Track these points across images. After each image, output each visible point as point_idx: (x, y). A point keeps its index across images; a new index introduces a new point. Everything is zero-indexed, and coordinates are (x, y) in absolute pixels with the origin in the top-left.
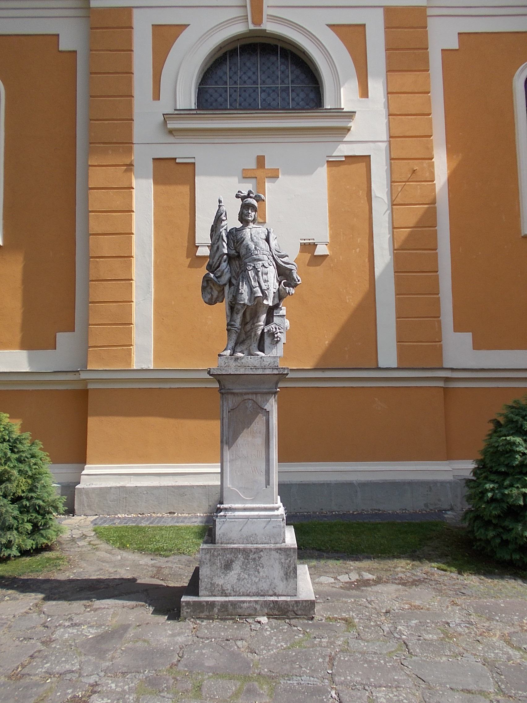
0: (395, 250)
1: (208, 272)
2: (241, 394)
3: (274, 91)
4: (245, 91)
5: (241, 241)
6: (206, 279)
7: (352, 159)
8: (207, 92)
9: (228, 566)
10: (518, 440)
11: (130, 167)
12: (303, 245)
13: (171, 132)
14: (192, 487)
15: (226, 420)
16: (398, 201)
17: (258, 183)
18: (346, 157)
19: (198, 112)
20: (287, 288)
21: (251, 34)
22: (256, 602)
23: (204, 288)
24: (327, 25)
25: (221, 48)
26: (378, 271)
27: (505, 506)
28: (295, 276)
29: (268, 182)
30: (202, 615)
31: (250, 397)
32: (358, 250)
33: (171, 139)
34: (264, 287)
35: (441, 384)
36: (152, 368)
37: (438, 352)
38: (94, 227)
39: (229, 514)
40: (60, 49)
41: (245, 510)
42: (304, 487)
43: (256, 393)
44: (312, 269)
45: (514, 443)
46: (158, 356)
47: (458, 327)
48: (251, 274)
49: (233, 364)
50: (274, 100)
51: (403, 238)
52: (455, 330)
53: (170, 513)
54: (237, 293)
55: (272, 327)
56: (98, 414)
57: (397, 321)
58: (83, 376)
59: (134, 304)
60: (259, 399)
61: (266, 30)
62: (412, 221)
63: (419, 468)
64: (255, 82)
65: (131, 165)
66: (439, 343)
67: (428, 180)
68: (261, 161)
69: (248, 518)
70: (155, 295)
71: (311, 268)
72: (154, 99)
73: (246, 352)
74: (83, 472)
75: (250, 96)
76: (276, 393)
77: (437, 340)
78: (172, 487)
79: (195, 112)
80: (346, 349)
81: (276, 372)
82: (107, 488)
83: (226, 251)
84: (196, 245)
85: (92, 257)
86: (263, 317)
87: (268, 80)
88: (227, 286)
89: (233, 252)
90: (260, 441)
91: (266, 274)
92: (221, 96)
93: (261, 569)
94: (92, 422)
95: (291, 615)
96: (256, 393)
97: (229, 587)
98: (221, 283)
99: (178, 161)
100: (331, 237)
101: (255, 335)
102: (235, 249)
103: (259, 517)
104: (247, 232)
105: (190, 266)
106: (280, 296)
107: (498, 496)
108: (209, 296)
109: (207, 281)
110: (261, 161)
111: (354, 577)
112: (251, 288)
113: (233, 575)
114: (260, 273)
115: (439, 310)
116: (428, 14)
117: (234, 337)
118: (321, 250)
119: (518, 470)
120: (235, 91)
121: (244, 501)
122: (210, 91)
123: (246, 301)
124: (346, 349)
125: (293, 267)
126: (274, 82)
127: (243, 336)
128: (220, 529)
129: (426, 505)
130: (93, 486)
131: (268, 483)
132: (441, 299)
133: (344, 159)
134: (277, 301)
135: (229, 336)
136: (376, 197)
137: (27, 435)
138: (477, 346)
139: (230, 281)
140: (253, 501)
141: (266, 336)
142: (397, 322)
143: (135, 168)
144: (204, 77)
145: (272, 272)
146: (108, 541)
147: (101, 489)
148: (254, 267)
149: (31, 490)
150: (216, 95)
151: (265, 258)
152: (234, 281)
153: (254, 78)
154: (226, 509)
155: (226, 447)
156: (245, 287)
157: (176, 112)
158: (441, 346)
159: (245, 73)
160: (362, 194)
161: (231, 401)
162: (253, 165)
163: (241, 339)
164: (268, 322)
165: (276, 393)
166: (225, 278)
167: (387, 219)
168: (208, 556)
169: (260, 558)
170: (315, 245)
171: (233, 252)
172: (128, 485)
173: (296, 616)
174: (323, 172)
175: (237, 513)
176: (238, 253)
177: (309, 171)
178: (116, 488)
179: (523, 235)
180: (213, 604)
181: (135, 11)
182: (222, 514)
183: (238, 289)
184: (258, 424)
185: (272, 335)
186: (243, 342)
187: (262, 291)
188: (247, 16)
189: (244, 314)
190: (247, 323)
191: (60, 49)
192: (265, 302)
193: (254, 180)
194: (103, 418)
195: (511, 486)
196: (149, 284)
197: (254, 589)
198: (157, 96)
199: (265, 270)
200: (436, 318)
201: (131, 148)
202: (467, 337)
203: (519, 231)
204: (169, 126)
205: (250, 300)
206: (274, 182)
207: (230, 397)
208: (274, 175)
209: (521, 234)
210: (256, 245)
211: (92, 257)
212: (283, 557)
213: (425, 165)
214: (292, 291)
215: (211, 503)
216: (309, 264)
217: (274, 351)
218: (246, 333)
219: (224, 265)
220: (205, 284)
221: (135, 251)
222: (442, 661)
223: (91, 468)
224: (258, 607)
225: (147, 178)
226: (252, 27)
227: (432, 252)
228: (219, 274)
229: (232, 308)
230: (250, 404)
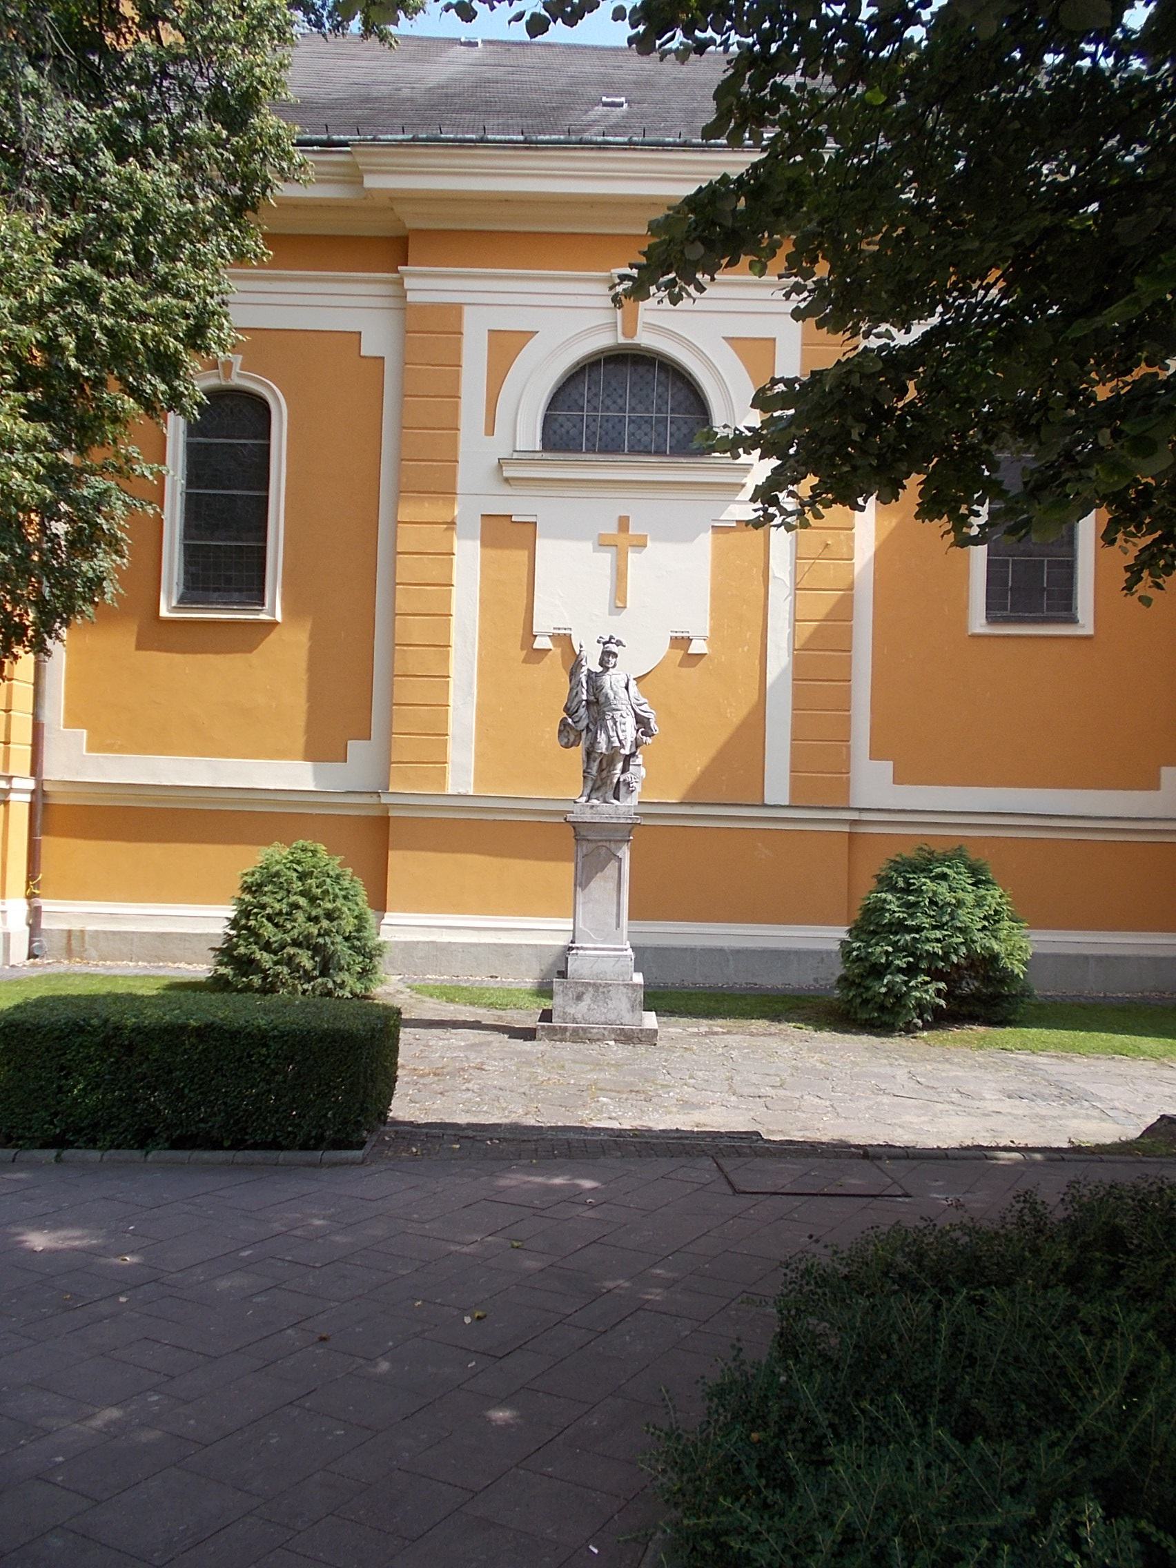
0: (795, 650)
2: (596, 841)
3: (646, 422)
4: (607, 421)
5: (600, 688)
6: (563, 722)
8: (556, 420)
9: (579, 998)
10: (890, 897)
11: (452, 524)
13: (507, 480)
14: (520, 945)
15: (580, 865)
16: (803, 585)
17: (618, 554)
22: (605, 1028)
23: (560, 732)
24: (724, 338)
26: (770, 678)
27: (867, 964)
28: (652, 725)
29: (632, 552)
30: (555, 1038)
31: (604, 844)
32: (746, 649)
33: (508, 490)
34: (621, 738)
35: (846, 829)
36: (471, 794)
37: (845, 787)
38: (402, 604)
39: (580, 952)
40: (362, 354)
41: (596, 949)
42: (661, 952)
43: (610, 841)
44: (685, 671)
45: (885, 900)
46: (479, 778)
47: (875, 755)
48: (610, 723)
49: (588, 811)
50: (646, 434)
51: (807, 634)
52: (873, 757)
53: (492, 977)
54: (594, 742)
55: (627, 776)
57: (792, 745)
58: (385, 799)
59: (450, 709)
60: (613, 846)
62: (822, 610)
63: (810, 934)
64: (622, 410)
65: (453, 523)
67: (844, 557)
68: (624, 523)
69: (598, 956)
70: (478, 697)
71: (684, 669)
72: (487, 434)
73: (601, 799)
75: (613, 427)
76: (628, 841)
77: (844, 771)
79: (538, 456)
80: (724, 778)
81: (630, 821)
82: (413, 942)
83: (584, 697)
85: (397, 645)
86: (620, 766)
87: (639, 407)
88: (585, 732)
89: (592, 698)
90: (612, 885)
92: (575, 426)
93: (609, 1002)
94: (394, 857)
95: (635, 1040)
96: (610, 841)
97: (580, 1016)
98: (579, 729)
100: (712, 630)
101: (612, 783)
102: (594, 695)
103: (609, 956)
104: (607, 680)
105: (525, 661)
106: (637, 744)
107: (863, 955)
108: (566, 740)
109: (565, 725)
110: (624, 523)
111: (703, 1029)
112: (609, 737)
113: (584, 1005)
114: (618, 724)
115: (848, 732)
117: (590, 784)
118: (697, 647)
119: (887, 929)
120: (594, 420)
121: (594, 942)
122: (560, 419)
123: (604, 751)
124: (724, 778)
125: (651, 716)
126: (647, 410)
127: (599, 783)
128: (571, 967)
129: (816, 980)
130: (396, 939)
131: (618, 925)
133: (734, 524)
134: (634, 750)
135: (584, 782)
137: (349, 870)
139: (587, 726)
140: (603, 942)
141: (621, 786)
143: (458, 527)
144: (553, 398)
145: (631, 721)
146: (431, 996)
147: (405, 943)
149: (358, 931)
150: (568, 425)
152: (591, 727)
153: (620, 401)
154: (578, 948)
155: (579, 889)
156: (603, 736)
157: (516, 456)
158: (848, 779)
159: (608, 396)
160: (757, 572)
161: (585, 848)
162: (612, 529)
163: (597, 786)
164: (624, 771)
165: (628, 841)
166: (583, 724)
167: (788, 608)
168: (561, 988)
169: (609, 992)
171: (592, 698)
172: (438, 940)
173: (641, 1042)
174: (707, 538)
175: (588, 952)
176: (597, 699)
178: (424, 943)
180: (565, 1029)
181: (466, 309)
182: (574, 952)
183: (596, 738)
184: (611, 868)
186: (598, 789)
187: (620, 741)
188: (616, 323)
189: (601, 761)
191: (362, 354)
192: (622, 751)
193: (614, 548)
194: (409, 854)
195: (877, 944)
196: (471, 683)
197: (603, 1019)
198: (490, 430)
199: (623, 720)
201: (454, 499)
202: (887, 767)
203: (966, 628)
204: (506, 474)
205: (607, 749)
206: (640, 553)
207: (584, 843)
208: (640, 544)
210: (615, 694)
211: (397, 645)
212: (630, 991)
214: (649, 740)
215: (543, 967)
216: (680, 665)
217: (629, 799)
218: (602, 780)
219: (582, 711)
220: (562, 728)
221: (454, 639)
223: (392, 917)
224: (606, 1033)
225: (473, 539)
226: (622, 340)
227: (844, 654)
228: (576, 720)
229: (590, 753)
230: (603, 851)
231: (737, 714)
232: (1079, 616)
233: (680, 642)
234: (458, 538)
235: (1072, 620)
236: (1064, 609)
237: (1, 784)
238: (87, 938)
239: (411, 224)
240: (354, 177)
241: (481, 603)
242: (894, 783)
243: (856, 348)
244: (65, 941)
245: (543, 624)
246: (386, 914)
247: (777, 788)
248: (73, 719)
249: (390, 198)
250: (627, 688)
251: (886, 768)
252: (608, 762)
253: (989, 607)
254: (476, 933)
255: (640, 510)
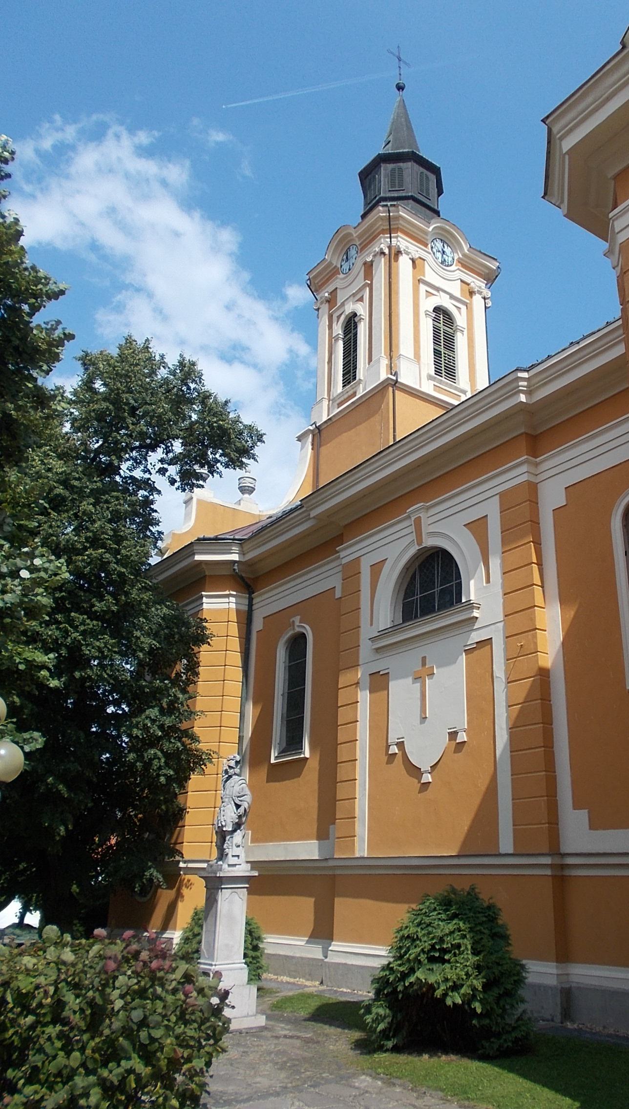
7: (481, 644)
21: (421, 552)
24: (464, 525)
25: (408, 569)
47: (576, 806)
58: (331, 863)
74: (330, 949)
78: (371, 967)
99: (381, 673)
118: (462, 737)
136: (497, 677)
138: (593, 826)
142: (514, 805)
143: (360, 684)
160: (488, 676)
177: (452, 661)
198: (371, 625)
202: (583, 814)
213: (530, 637)
222: (85, 617)
231: (483, 784)
233: (453, 735)
234: (360, 690)
242: (591, 828)
243: (354, 394)
245: (393, 738)
246: (333, 943)
247: (506, 844)
249: (328, 517)
251: (583, 815)
254: (365, 958)
255: (429, 649)
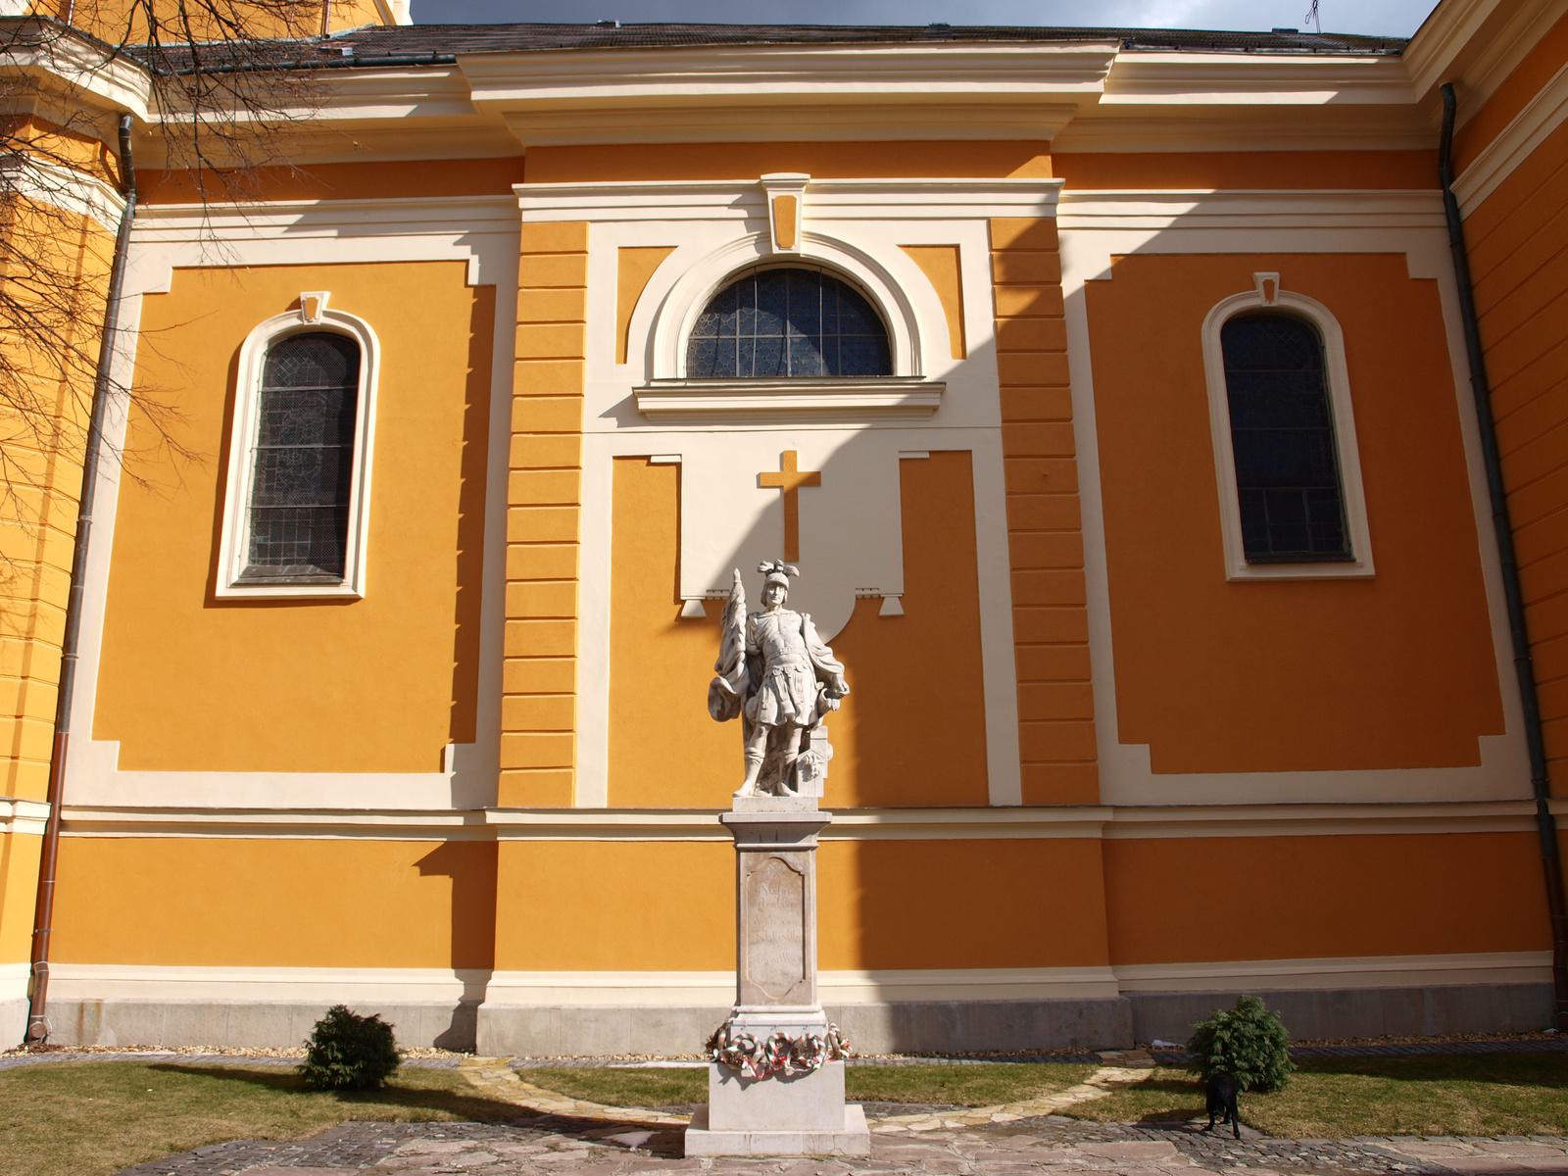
1: (717, 674)
12: (861, 600)
18: (930, 452)
19: (688, 384)
20: (830, 700)
23: (711, 700)
24: (900, 246)
35: (1097, 834)
38: (513, 568)
47: (1126, 737)
48: (780, 681)
56: (56, 961)
61: (799, 254)
66: (1091, 764)
84: (682, 598)
91: (801, 681)
112: (779, 701)
114: (791, 681)
116: (1059, 225)
132: (1094, 687)
133: (927, 456)
145: (809, 676)
148: (783, 672)
151: (799, 659)
164: (804, 748)
170: (881, 599)
179: (1228, 578)
181: (591, 227)
185: (808, 769)
190: (774, 749)
200: (1087, 717)
202: (1141, 753)
209: (1224, 577)
232: (1356, 554)
235: (1345, 557)
236: (1335, 547)
237: (3, 809)
238: (104, 1014)
239: (528, 141)
240: (458, 93)
241: (614, 563)
242: (1153, 772)
244: (75, 1018)
247: (1005, 779)
248: (103, 731)
250: (802, 632)
252: (780, 734)
253: (818, 963)
